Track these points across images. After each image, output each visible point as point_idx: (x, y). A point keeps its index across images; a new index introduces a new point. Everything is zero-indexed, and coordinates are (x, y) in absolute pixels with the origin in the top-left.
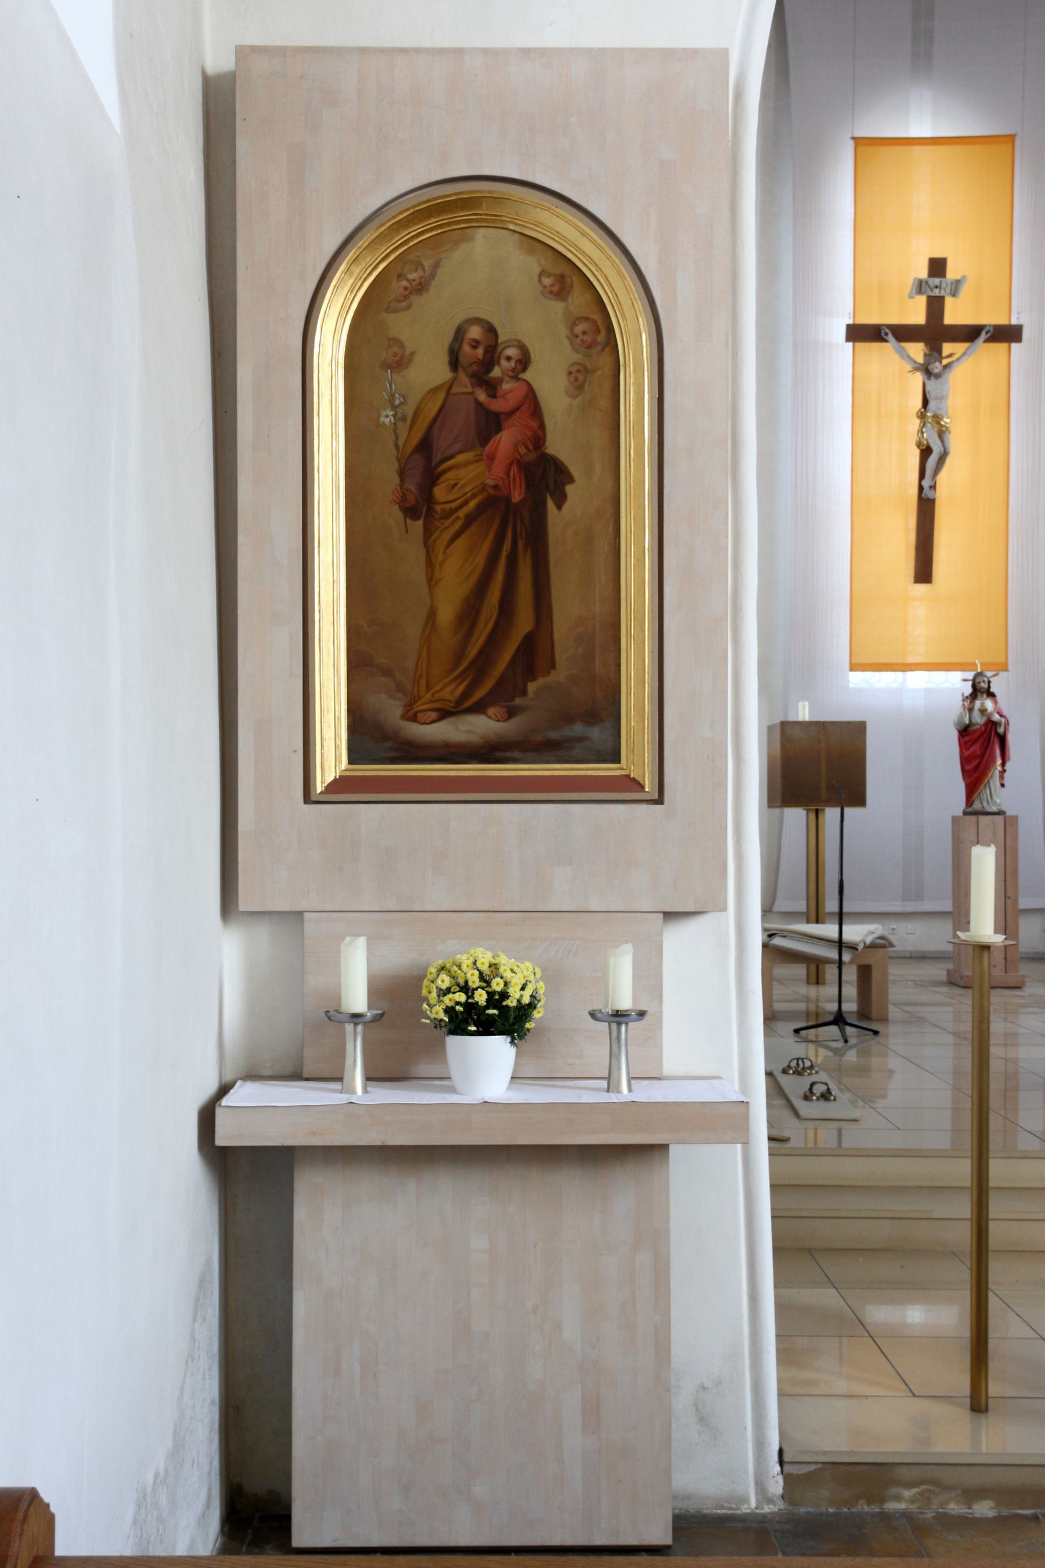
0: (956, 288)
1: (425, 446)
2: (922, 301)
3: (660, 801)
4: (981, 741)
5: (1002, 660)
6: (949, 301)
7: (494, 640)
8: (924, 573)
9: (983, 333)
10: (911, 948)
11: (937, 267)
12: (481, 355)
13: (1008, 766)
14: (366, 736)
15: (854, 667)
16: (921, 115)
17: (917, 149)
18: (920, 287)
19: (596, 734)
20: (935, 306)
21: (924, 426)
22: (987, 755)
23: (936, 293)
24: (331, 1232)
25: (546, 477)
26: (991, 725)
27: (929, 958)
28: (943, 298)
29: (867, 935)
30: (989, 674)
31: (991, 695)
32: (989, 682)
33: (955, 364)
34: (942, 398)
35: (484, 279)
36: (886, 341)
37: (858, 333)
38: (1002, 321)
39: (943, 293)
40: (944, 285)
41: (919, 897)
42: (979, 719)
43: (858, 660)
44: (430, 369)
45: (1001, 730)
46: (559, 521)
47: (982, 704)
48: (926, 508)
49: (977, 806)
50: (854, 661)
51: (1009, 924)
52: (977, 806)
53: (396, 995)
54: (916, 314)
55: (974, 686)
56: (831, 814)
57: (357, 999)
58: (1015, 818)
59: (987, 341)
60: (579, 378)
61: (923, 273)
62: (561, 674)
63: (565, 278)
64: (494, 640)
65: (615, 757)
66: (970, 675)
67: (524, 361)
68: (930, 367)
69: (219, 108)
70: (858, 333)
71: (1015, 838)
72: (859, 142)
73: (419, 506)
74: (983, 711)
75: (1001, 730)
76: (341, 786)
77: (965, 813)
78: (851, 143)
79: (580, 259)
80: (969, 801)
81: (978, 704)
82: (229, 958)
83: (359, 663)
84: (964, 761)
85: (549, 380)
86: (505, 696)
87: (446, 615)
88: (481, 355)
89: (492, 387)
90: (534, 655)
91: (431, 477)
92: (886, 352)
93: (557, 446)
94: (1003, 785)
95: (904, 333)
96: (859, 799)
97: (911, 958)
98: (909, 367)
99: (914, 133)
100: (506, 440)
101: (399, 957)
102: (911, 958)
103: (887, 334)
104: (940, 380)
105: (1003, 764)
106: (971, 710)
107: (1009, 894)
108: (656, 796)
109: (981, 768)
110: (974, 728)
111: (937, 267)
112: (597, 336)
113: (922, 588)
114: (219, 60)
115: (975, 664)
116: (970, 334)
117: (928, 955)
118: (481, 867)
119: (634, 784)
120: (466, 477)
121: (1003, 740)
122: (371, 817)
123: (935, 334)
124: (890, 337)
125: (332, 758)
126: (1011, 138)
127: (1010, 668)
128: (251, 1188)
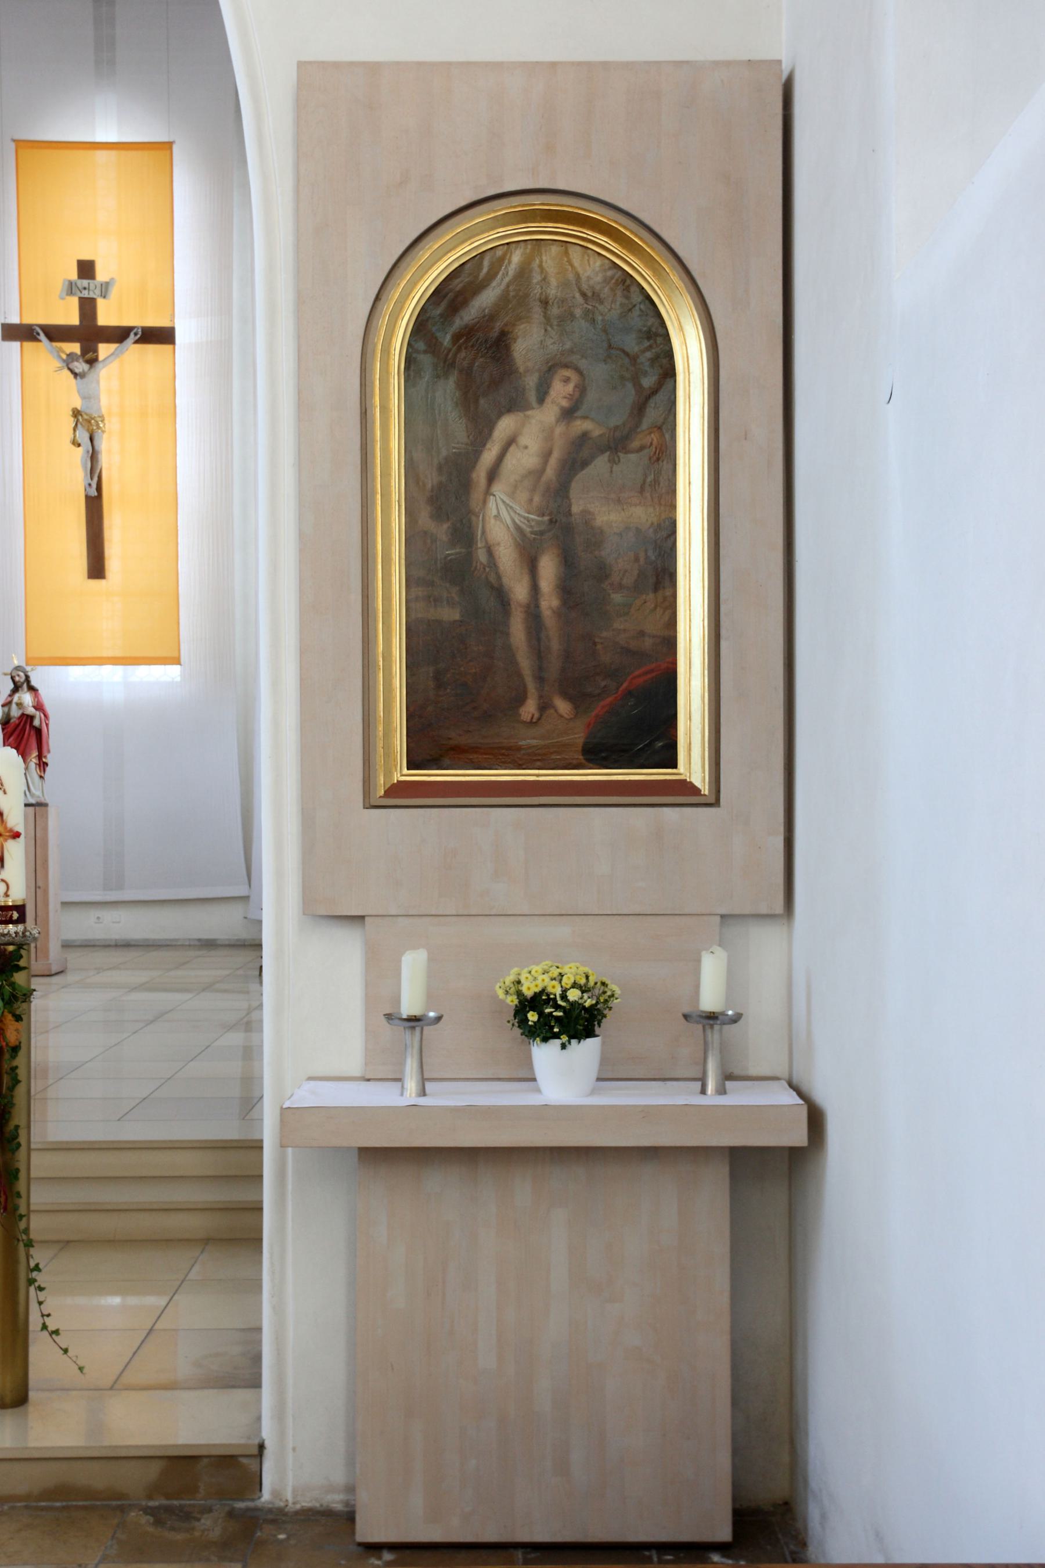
0: (105, 289)
2: (74, 302)
3: (716, 803)
4: (17, 733)
5: (175, 655)
6: (101, 303)
8: (97, 569)
9: (132, 335)
10: (117, 937)
11: (86, 269)
13: (49, 759)
16: (107, 121)
17: (101, 155)
18: (71, 288)
20: (88, 307)
23: (85, 294)
27: (134, 946)
31: (32, 689)
36: (40, 341)
39: (92, 295)
40: (92, 287)
41: (120, 887)
42: (15, 713)
45: (36, 723)
47: (20, 698)
48: (94, 506)
51: (39, 913)
54: (69, 315)
59: (136, 342)
61: (73, 275)
65: (671, 762)
68: (71, 366)
72: (21, 144)
74: (20, 705)
78: (13, 145)
79: (654, 289)
92: (44, 358)
95: (55, 334)
97: (116, 946)
99: (101, 137)
102: (116, 946)
104: (85, 380)
105: (40, 756)
107: (39, 884)
108: (712, 800)
111: (86, 269)
116: (120, 335)
117: (133, 943)
119: (686, 788)
121: (38, 732)
123: (88, 338)
124: (42, 337)
127: (182, 661)
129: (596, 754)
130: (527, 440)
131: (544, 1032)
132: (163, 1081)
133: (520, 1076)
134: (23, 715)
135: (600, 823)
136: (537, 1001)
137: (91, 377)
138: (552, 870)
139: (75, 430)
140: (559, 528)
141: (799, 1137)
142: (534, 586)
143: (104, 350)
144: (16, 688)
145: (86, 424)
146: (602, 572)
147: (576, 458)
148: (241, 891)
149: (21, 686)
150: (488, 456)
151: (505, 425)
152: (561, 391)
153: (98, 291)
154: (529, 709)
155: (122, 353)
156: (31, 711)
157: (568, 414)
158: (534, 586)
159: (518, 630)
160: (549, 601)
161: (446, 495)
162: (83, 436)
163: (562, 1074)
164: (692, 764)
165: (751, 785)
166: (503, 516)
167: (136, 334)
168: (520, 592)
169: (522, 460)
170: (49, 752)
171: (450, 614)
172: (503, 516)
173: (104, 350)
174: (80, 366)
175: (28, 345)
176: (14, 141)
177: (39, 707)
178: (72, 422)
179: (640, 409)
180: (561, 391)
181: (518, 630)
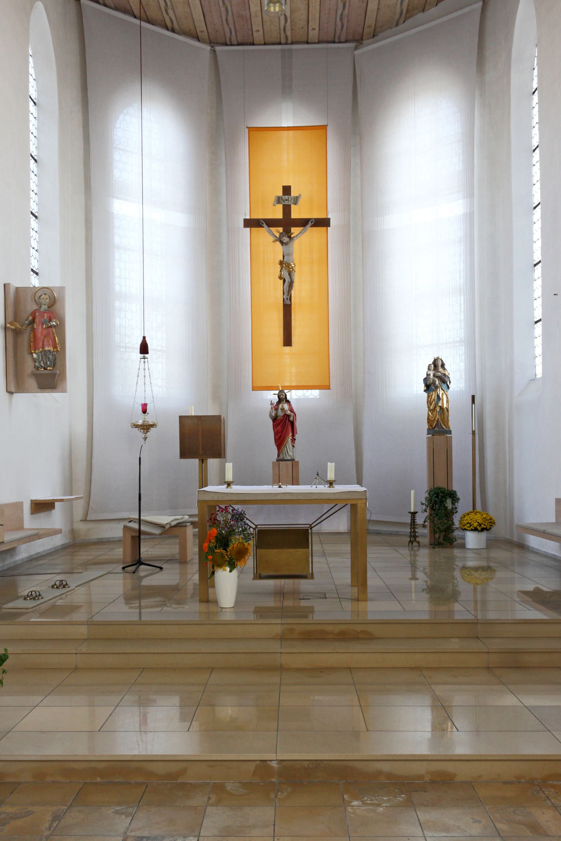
0: (296, 200)
2: (280, 207)
4: (282, 423)
8: (288, 341)
9: (310, 223)
11: (287, 190)
13: (297, 437)
15: (253, 389)
16: (287, 115)
17: (285, 133)
18: (279, 200)
20: (287, 210)
21: (282, 268)
22: (284, 431)
23: (286, 203)
26: (287, 416)
28: (290, 205)
29: (173, 521)
30: (286, 391)
31: (288, 402)
32: (286, 395)
33: (295, 238)
34: (289, 255)
37: (250, 223)
38: (322, 216)
39: (290, 203)
40: (290, 199)
42: (280, 414)
43: (258, 384)
45: (291, 419)
48: (287, 309)
49: (281, 457)
50: (254, 385)
52: (281, 457)
54: (278, 214)
55: (279, 397)
58: (298, 462)
59: (311, 226)
66: (277, 392)
68: (282, 239)
70: (250, 223)
71: (298, 472)
72: (251, 129)
74: (283, 409)
75: (291, 419)
77: (277, 460)
78: (247, 130)
80: (279, 456)
81: (280, 406)
84: (276, 434)
92: (265, 236)
94: (293, 446)
95: (271, 223)
98: (272, 239)
99: (284, 125)
103: (263, 224)
105: (293, 436)
106: (276, 409)
109: (281, 438)
110: (279, 418)
111: (287, 190)
113: (287, 348)
115: (278, 387)
116: (303, 223)
121: (292, 424)
123: (287, 226)
124: (265, 225)
126: (325, 127)
132: (40, 705)
133: (154, 763)
134: (285, 414)
137: (290, 244)
139: (281, 271)
143: (295, 231)
149: (283, 401)
153: (292, 201)
155: (305, 232)
156: (289, 412)
162: (285, 274)
167: (312, 222)
170: (297, 433)
173: (295, 231)
174: (286, 239)
176: (247, 127)
177: (292, 410)
178: (279, 267)
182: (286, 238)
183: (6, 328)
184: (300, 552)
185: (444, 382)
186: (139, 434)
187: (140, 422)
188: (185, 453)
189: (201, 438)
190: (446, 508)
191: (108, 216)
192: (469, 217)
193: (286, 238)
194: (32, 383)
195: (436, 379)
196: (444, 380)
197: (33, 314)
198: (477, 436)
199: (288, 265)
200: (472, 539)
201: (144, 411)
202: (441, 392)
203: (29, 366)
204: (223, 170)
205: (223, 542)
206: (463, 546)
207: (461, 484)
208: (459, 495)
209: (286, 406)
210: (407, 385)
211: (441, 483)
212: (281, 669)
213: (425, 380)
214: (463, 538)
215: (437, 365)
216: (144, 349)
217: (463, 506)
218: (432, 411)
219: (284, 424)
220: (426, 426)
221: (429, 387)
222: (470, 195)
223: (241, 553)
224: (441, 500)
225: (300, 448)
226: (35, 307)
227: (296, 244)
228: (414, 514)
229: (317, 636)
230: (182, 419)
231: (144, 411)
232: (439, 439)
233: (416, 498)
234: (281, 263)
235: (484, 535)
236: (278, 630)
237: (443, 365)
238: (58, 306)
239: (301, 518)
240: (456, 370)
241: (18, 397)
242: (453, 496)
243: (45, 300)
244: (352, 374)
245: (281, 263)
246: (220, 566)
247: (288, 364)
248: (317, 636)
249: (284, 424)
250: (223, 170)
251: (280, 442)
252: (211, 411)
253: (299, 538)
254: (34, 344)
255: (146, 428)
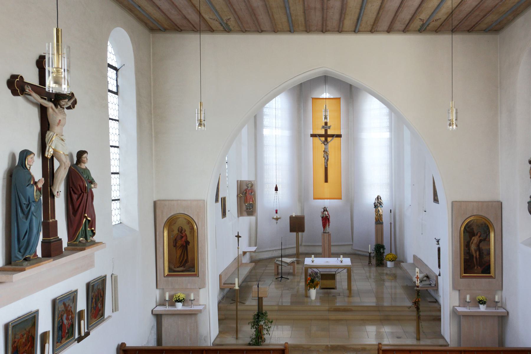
0: (329, 127)
1: (176, 239)
7: (183, 259)
8: (326, 181)
12: (181, 230)
14: (170, 270)
15: (314, 199)
18: (323, 127)
19: (193, 269)
20: (326, 131)
24: (166, 322)
25: (187, 243)
35: (181, 223)
37: (313, 136)
42: (324, 216)
44: (176, 232)
46: (189, 247)
53: (171, 297)
54: (323, 132)
56: (300, 233)
57: (167, 299)
60: (191, 232)
62: (189, 263)
63: (189, 223)
64: (183, 259)
67: (185, 231)
69: (155, 203)
70: (313, 136)
73: (175, 246)
76: (168, 276)
82: (158, 292)
83: (169, 262)
85: (188, 233)
86: (184, 266)
87: (178, 257)
88: (181, 230)
89: (182, 233)
90: (186, 261)
91: (176, 243)
92: (317, 139)
93: (188, 239)
95: (320, 136)
96: (303, 231)
100: (184, 239)
101: (172, 293)
112: (192, 228)
114: (155, 200)
116: (332, 136)
118: (182, 284)
120: (179, 243)
121: (329, 219)
122: (170, 279)
123: (326, 136)
125: (167, 272)
126: (340, 98)
128: (158, 317)
129: (482, 273)
130: (475, 239)
131: (481, 304)
135: (484, 280)
136: (481, 301)
138: (479, 285)
140: (479, 249)
141: (506, 315)
142: (476, 254)
143: (329, 139)
144: (324, 211)
145: (325, 152)
146: (483, 253)
147: (481, 241)
148: (351, 243)
150: (472, 241)
151: (473, 238)
152: (479, 234)
154: (476, 268)
157: (479, 237)
158: (476, 254)
159: (475, 259)
160: (478, 256)
161: (467, 245)
163: (482, 308)
164: (492, 274)
165: (498, 276)
166: (473, 247)
168: (475, 255)
169: (475, 242)
171: (468, 258)
172: (473, 247)
173: (329, 139)
174: (326, 143)
175: (314, 138)
177: (328, 214)
178: (323, 153)
179: (487, 235)
180: (479, 234)
181: (475, 259)
182: (326, 142)
183: (237, 196)
184: (333, 281)
185: (381, 205)
186: (275, 221)
187: (275, 217)
188: (292, 230)
189: (297, 224)
190: (381, 252)
191: (262, 135)
192: (391, 139)
193: (326, 142)
194: (245, 213)
195: (378, 203)
196: (380, 204)
197: (246, 190)
198: (393, 225)
199: (326, 152)
200: (389, 264)
201: (277, 213)
202: (379, 208)
203: (244, 208)
204: (302, 111)
205: (312, 281)
206: (386, 266)
207: (386, 243)
208: (385, 247)
209: (326, 213)
210: (371, 200)
211: (380, 243)
212: (329, 320)
213: (375, 203)
214: (386, 263)
215: (378, 198)
216: (276, 189)
217: (387, 251)
218: (377, 215)
219: (326, 220)
220: (375, 221)
221: (376, 206)
222: (391, 131)
223: (317, 285)
224: (379, 248)
225: (332, 227)
226: (246, 187)
227: (329, 144)
228: (370, 253)
229: (338, 310)
230: (291, 218)
231: (277, 213)
232: (379, 226)
233: (371, 248)
234: (324, 151)
235: (393, 262)
236: (327, 308)
237: (380, 198)
238: (253, 187)
239: (333, 271)
240: (385, 199)
241: (241, 218)
242: (383, 247)
243: (250, 185)
244: (350, 194)
245: (324, 151)
246: (312, 288)
247: (327, 189)
248: (338, 310)
249: (326, 220)
250: (302, 111)
251: (324, 226)
252: (299, 214)
253: (332, 277)
254: (246, 201)
255: (277, 219)
